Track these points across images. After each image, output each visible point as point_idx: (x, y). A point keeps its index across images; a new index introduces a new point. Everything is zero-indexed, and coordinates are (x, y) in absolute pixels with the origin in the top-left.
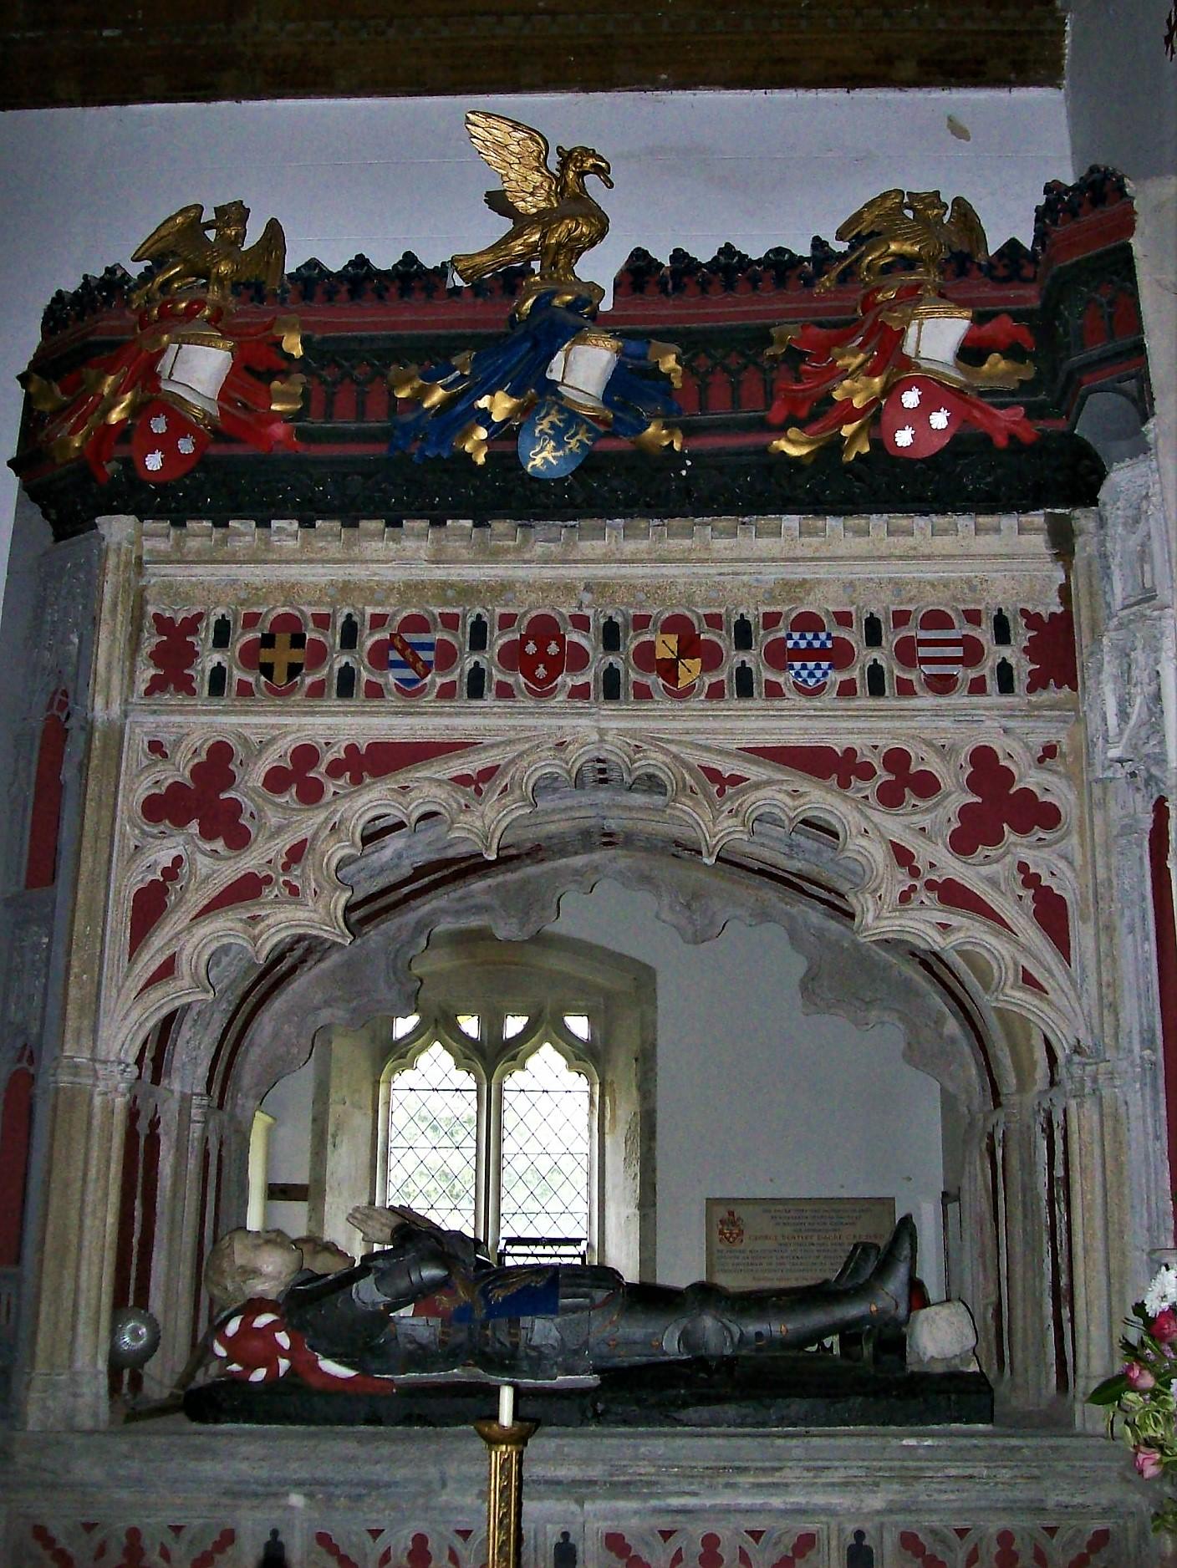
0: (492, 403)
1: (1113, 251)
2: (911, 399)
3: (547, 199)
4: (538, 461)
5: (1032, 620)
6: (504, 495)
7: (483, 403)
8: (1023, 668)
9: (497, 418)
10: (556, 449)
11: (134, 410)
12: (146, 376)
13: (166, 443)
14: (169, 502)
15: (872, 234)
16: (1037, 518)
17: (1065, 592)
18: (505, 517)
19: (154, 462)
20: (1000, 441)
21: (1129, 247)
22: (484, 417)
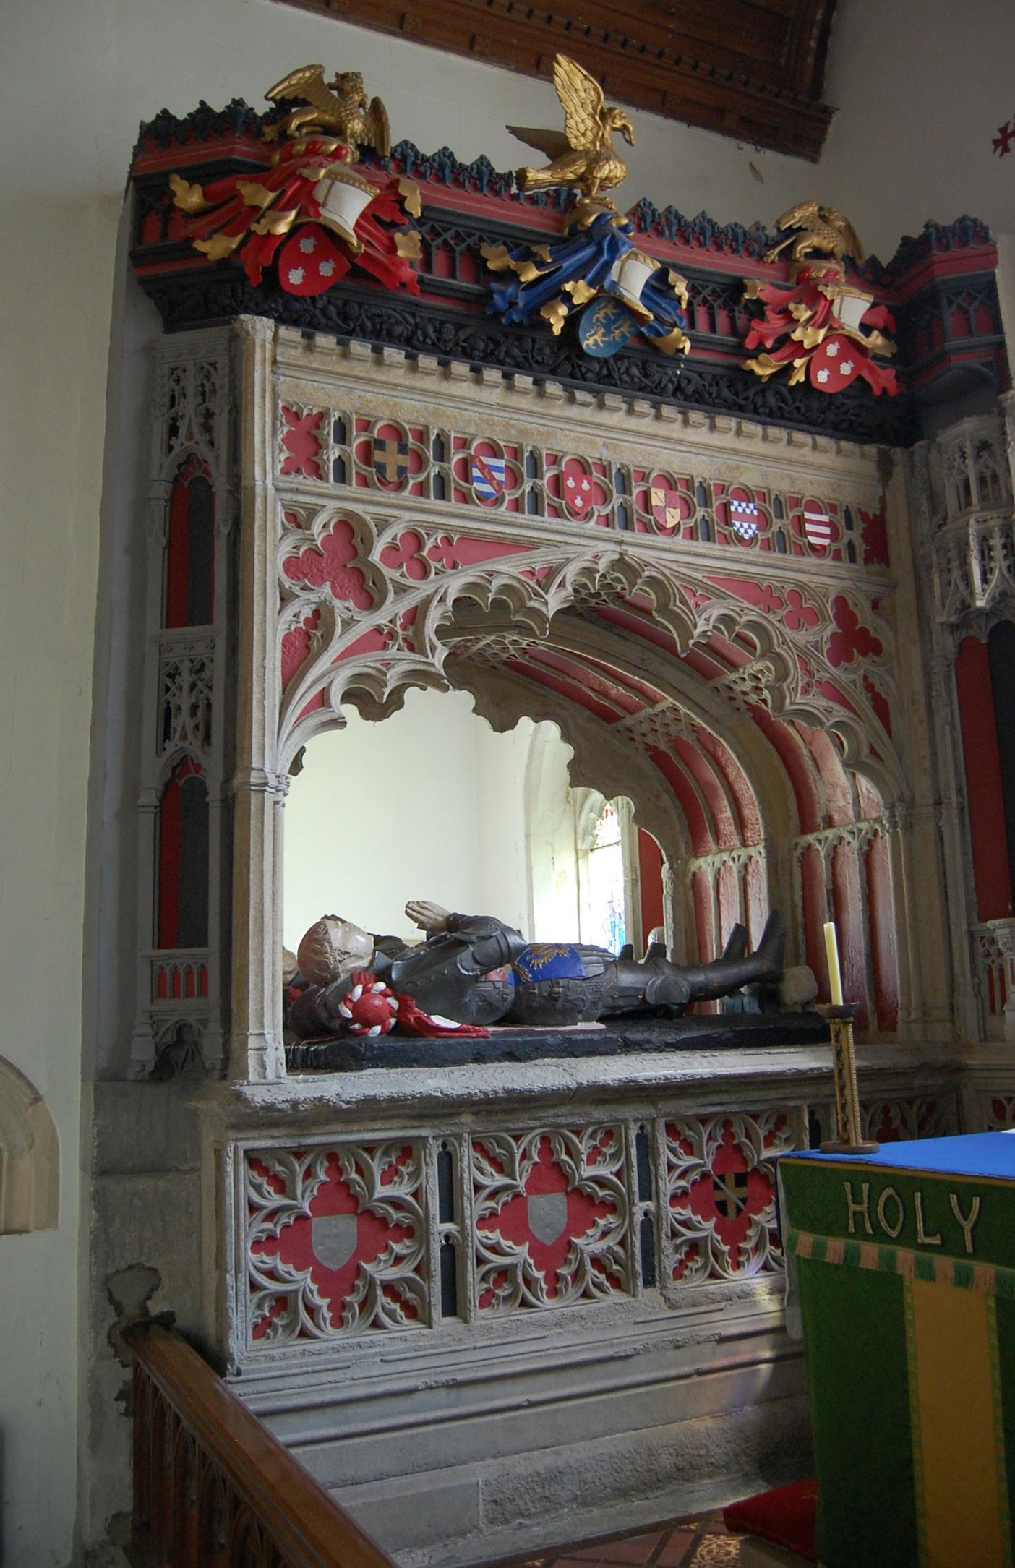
0: (575, 288)
1: (986, 275)
2: (832, 350)
3: (593, 142)
4: (591, 342)
5: (864, 516)
6: (564, 363)
7: (568, 287)
8: (861, 547)
9: (576, 301)
10: (604, 335)
11: (295, 229)
12: (306, 198)
13: (309, 264)
14: (300, 314)
15: (800, 229)
16: (871, 450)
17: (883, 500)
18: (970, 415)
19: (296, 277)
20: (877, 391)
21: (994, 275)
22: (567, 297)
